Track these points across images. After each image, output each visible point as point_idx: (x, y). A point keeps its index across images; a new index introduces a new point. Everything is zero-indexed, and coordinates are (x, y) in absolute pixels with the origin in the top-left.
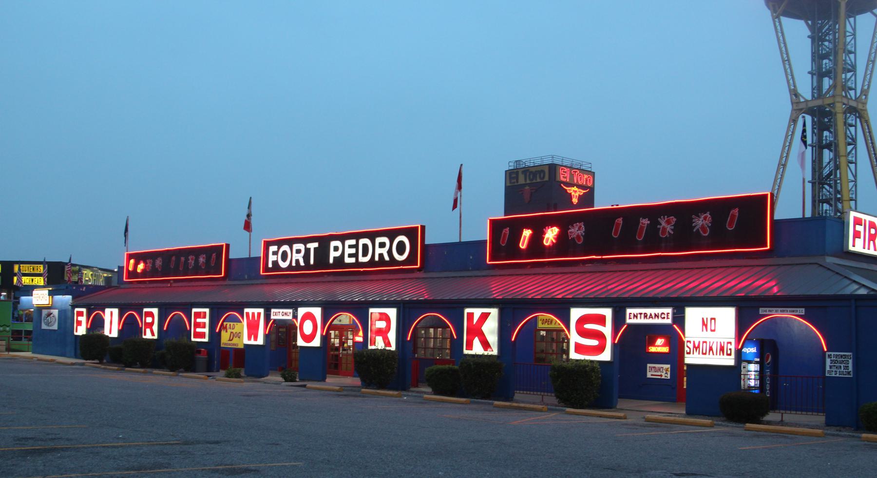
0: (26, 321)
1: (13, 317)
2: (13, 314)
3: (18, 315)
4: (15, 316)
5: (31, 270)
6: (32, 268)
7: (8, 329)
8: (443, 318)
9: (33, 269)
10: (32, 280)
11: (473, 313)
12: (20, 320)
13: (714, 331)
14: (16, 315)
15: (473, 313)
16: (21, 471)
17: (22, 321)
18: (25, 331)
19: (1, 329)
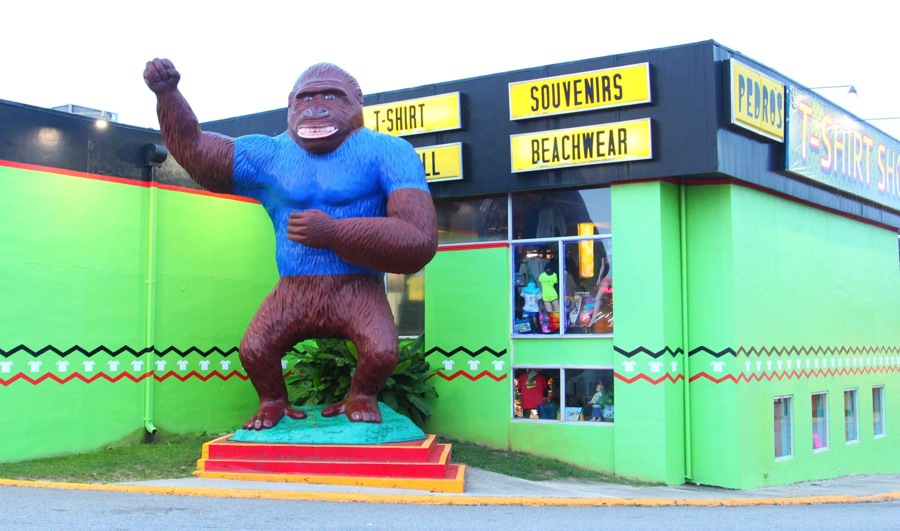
0: (569, 330)
1: (519, 314)
2: (519, 301)
3: (541, 302)
4: (526, 308)
5: (582, 97)
6: (581, 87)
7: (498, 366)
8: (388, 463)
9: (589, 91)
10: (588, 141)
11: (674, 357)
12: (545, 328)
13: (533, 141)
14: (531, 306)
15: (674, 357)
16: (207, 511)
17: (555, 330)
18: (570, 373)
19: (4, 367)
